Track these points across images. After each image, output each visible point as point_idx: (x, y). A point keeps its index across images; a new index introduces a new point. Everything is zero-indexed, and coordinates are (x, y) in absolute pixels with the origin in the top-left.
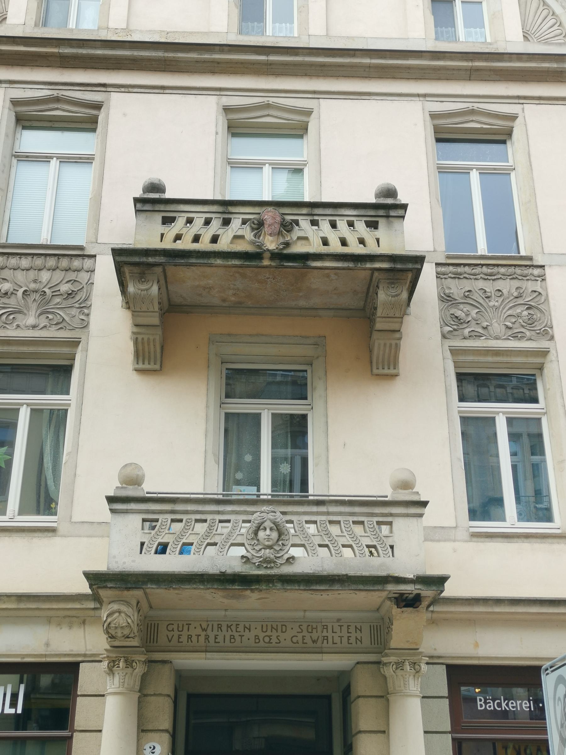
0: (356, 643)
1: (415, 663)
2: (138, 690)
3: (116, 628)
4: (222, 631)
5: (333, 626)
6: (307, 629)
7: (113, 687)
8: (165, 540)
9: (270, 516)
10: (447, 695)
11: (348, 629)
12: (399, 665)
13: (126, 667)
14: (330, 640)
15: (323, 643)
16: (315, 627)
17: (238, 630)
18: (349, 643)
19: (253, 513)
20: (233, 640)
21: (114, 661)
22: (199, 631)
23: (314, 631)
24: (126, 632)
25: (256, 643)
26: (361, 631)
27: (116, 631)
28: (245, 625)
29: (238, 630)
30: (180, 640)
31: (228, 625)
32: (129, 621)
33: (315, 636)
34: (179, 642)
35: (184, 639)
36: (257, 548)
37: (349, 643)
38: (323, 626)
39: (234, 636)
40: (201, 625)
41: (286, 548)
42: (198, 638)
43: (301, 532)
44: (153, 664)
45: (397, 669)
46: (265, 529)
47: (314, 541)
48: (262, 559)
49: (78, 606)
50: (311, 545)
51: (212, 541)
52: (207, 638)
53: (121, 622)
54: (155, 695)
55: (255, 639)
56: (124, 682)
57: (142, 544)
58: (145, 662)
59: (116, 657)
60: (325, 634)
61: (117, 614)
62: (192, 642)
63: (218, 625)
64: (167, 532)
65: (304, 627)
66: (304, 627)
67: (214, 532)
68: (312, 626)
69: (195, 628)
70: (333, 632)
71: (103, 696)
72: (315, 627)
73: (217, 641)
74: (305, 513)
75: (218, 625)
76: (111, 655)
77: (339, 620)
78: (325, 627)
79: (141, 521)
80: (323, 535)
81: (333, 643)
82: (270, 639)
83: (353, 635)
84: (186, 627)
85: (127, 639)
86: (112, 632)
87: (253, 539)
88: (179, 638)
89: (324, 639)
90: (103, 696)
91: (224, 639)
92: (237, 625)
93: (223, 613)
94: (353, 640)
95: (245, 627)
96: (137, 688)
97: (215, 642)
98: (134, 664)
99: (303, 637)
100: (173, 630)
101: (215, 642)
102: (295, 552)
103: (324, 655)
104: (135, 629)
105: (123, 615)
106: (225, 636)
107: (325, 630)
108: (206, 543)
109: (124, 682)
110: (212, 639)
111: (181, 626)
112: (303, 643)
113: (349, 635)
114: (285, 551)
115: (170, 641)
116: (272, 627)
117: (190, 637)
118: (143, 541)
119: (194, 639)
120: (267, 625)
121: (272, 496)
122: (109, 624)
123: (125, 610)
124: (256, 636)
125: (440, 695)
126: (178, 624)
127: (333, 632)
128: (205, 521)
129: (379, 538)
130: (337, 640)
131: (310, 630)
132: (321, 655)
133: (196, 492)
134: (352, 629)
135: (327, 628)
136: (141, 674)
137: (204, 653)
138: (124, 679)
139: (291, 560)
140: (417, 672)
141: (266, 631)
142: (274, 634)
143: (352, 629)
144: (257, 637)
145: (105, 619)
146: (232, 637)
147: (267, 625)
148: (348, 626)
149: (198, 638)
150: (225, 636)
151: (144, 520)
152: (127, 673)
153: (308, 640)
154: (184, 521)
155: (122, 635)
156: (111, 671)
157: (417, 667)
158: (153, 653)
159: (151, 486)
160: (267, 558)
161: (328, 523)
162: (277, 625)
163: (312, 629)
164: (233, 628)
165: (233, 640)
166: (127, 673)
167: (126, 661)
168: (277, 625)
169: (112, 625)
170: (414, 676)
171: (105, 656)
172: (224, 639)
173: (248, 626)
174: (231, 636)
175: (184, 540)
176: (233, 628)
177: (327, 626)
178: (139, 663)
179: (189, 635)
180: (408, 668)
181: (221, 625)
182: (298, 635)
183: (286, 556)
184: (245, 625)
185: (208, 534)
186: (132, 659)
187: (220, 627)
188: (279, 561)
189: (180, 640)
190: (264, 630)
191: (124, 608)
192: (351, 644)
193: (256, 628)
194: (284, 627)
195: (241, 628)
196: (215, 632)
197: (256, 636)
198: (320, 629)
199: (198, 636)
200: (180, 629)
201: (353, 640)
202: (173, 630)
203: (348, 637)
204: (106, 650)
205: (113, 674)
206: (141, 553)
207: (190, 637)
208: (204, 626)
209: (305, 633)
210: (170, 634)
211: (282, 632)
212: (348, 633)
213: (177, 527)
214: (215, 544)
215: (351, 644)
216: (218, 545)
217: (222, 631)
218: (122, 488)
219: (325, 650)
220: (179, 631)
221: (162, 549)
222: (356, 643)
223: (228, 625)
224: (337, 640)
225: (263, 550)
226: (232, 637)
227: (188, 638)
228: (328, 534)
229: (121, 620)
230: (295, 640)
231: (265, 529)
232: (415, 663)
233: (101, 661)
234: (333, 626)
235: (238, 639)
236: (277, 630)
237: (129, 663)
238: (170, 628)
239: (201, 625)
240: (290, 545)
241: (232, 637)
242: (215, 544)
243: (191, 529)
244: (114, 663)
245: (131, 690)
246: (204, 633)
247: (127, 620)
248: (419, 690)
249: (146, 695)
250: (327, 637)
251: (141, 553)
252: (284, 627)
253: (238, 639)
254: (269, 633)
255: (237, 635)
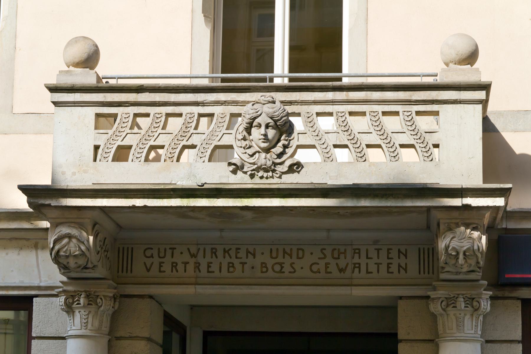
0: (399, 272)
1: (473, 299)
2: (107, 333)
3: (67, 257)
4: (217, 257)
5: (367, 250)
6: (332, 254)
7: (73, 328)
8: (126, 143)
9: (268, 109)
10: (520, 339)
11: (389, 253)
12: (451, 302)
13: (88, 304)
14: (363, 268)
15: (353, 272)
16: (342, 250)
17: (239, 255)
18: (388, 272)
19: (244, 103)
20: (231, 269)
21: (73, 297)
22: (186, 257)
23: (342, 256)
24: (82, 262)
25: (262, 272)
26: (406, 256)
27: (68, 260)
28: (247, 249)
29: (239, 255)
30: (162, 269)
31: (224, 249)
32: (83, 248)
33: (342, 263)
34: (160, 271)
35: (167, 267)
36: (250, 151)
37: (388, 272)
38: (355, 250)
39: (233, 264)
40: (189, 249)
41: (289, 151)
42: (185, 267)
43: (311, 129)
44: (127, 300)
45: (448, 306)
46: (259, 126)
47: (328, 141)
48: (256, 166)
49: (26, 225)
50: (325, 146)
51: (189, 143)
52: (197, 266)
53: (73, 250)
54: (131, 338)
55: (262, 267)
56: (87, 322)
57: (97, 148)
58: (115, 298)
59: (75, 292)
60: (356, 260)
61: (66, 241)
62: (177, 271)
63: (212, 249)
64: (129, 131)
65: (328, 252)
66: (328, 252)
67: (192, 131)
68: (339, 249)
69: (182, 253)
70: (367, 258)
71: (63, 338)
72: (342, 250)
73: (210, 270)
74: (315, 102)
75: (212, 249)
76: (70, 288)
77: (376, 242)
78: (357, 251)
79: (93, 117)
80: (340, 132)
81: (368, 272)
82: (282, 267)
83: (395, 263)
84: (169, 252)
85: (85, 270)
86: (63, 261)
87: (244, 139)
88: (161, 266)
89: (355, 267)
90: (63, 338)
91: (220, 268)
92: (238, 249)
93: (218, 234)
94: (394, 268)
95: (248, 252)
96: (106, 329)
97: (208, 272)
98: (99, 300)
99: (327, 264)
100: (152, 256)
101: (208, 272)
102: (302, 156)
103: (353, 288)
104: (94, 258)
105: (74, 240)
106: (221, 263)
107: (357, 256)
108: (147, 147)
109: (87, 322)
110: (203, 267)
111: (162, 250)
112: (327, 272)
113: (390, 261)
114: (288, 155)
115: (148, 270)
116: (285, 252)
117: (174, 265)
118: (97, 143)
119: (181, 267)
120: (277, 249)
121: (212, 79)
122: (58, 251)
123: (77, 234)
124: (262, 263)
125: (511, 339)
126: (159, 249)
127: (367, 258)
128: (180, 115)
129: (385, 135)
130: (373, 268)
131: (336, 256)
132: (349, 288)
133: (150, 74)
134: (394, 254)
135: (359, 253)
136: (110, 312)
137: (193, 286)
138: (87, 318)
139: (296, 167)
140: (476, 310)
141: (276, 258)
142: (287, 261)
143: (394, 254)
144: (264, 265)
145: (52, 246)
146: (231, 265)
147: (277, 249)
148: (388, 250)
149: (185, 267)
150: (221, 263)
151: (98, 115)
152: (90, 312)
153: (333, 268)
154: (152, 116)
155: (75, 266)
156: (69, 309)
157: (475, 304)
158: (126, 286)
159: (108, 68)
160: (262, 166)
161: (347, 115)
162: (291, 249)
163: (340, 254)
164: (233, 253)
165: (231, 269)
166: (90, 312)
167: (88, 296)
168: (291, 249)
169: (62, 253)
170: (472, 315)
171: (61, 289)
172: (220, 268)
173: (251, 250)
174: (229, 263)
175: (152, 143)
176: (233, 253)
177: (359, 249)
178: (106, 299)
179: (173, 263)
180: (463, 305)
181: (216, 249)
182: (319, 261)
183: (288, 163)
184: (247, 249)
185: (184, 132)
186: (97, 294)
187: (214, 252)
188: (279, 169)
189: (162, 269)
190: (274, 255)
191: (74, 232)
192: (392, 273)
193: (263, 254)
194: (300, 252)
195: (242, 254)
196: (208, 259)
197: (262, 263)
198: (349, 254)
199: (186, 263)
200: (162, 255)
201: (394, 268)
202: (152, 256)
203: (388, 264)
204: (62, 282)
205: (73, 312)
206: (95, 160)
207: (174, 265)
208: (193, 250)
209: (329, 259)
210: (149, 262)
211: (298, 258)
212: (388, 258)
213: (175, 124)
214: (193, 147)
215: (392, 273)
216: (198, 148)
217: (217, 257)
218: (67, 72)
219: (355, 282)
220: (160, 257)
221: (122, 154)
222: (399, 272)
223: (224, 249)
224: (373, 268)
225: (257, 155)
226: (231, 265)
227: (172, 266)
228: (347, 130)
229: (73, 248)
230: (315, 268)
231: (259, 126)
232: (473, 299)
233: (56, 296)
234: (367, 250)
235: (238, 267)
236: (291, 256)
237: (92, 299)
238: (148, 253)
239: (189, 249)
240: (294, 147)
241: (231, 265)
242: (193, 147)
243: (161, 127)
244: (73, 300)
245: (98, 330)
246: (194, 260)
247: (80, 247)
248: (480, 333)
249: (118, 338)
250: (359, 264)
251: (95, 160)
252: (300, 252)
253: (238, 267)
254: (280, 260)
255: (236, 262)
